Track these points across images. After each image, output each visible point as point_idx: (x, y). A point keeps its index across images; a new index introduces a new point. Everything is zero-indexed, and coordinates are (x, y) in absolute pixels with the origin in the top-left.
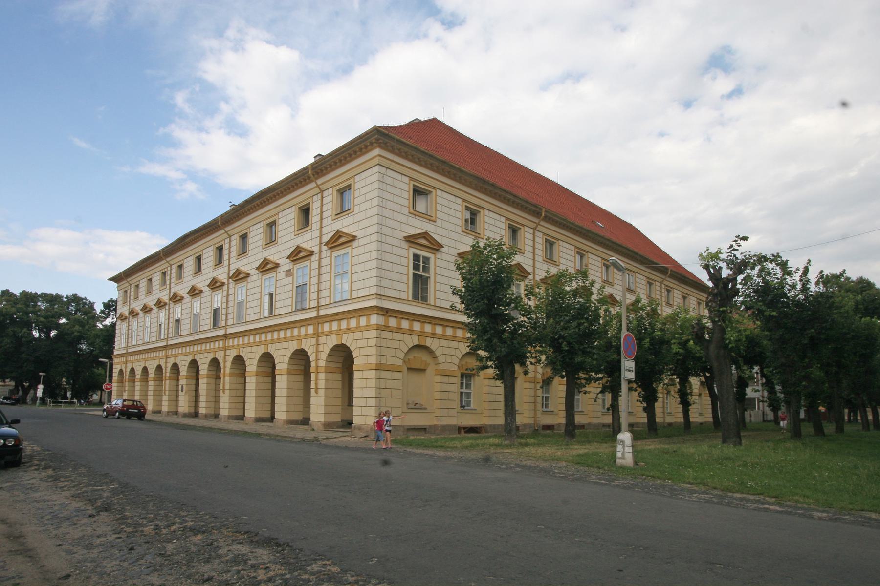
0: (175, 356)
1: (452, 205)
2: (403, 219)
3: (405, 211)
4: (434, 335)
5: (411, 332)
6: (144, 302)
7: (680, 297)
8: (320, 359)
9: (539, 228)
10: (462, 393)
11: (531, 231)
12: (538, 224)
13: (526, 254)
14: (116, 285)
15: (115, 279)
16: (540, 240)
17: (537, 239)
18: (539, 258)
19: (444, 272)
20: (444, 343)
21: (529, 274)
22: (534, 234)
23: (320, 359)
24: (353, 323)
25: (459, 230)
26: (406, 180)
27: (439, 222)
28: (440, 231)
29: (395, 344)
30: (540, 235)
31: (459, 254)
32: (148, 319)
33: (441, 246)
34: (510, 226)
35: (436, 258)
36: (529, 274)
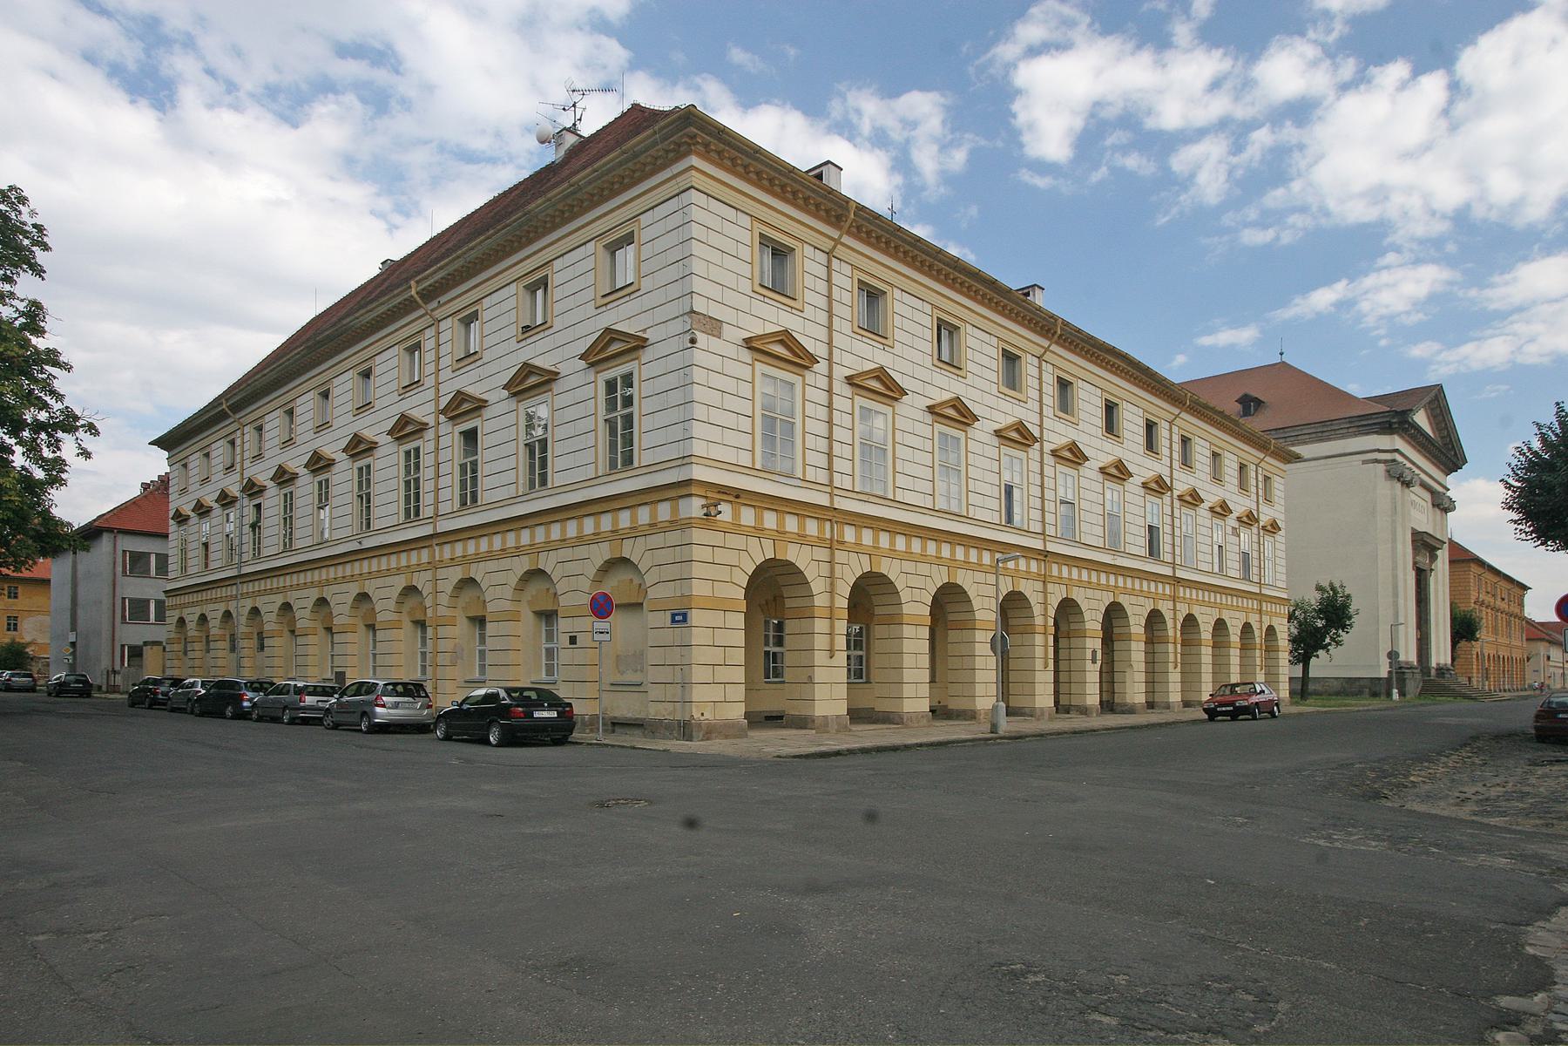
0: (183, 606)
1: (729, 229)
2: (743, 303)
3: (928, 362)
4: (892, 554)
5: (758, 531)
6: (221, 485)
7: (1208, 453)
8: (1042, 614)
9: (1178, 421)
10: (767, 653)
11: (822, 258)
12: (837, 242)
13: (1030, 404)
14: (166, 454)
15: (160, 443)
16: (844, 279)
17: (1045, 377)
18: (1176, 465)
19: (910, 440)
20: (909, 566)
21: (814, 360)
22: (1040, 367)
23: (1042, 614)
24: (644, 515)
25: (746, 286)
26: (745, 221)
27: (898, 348)
28: (975, 395)
29: (731, 557)
30: (847, 269)
31: (747, 341)
32: (206, 527)
33: (904, 392)
34: (764, 240)
35: (804, 384)
36: (814, 360)
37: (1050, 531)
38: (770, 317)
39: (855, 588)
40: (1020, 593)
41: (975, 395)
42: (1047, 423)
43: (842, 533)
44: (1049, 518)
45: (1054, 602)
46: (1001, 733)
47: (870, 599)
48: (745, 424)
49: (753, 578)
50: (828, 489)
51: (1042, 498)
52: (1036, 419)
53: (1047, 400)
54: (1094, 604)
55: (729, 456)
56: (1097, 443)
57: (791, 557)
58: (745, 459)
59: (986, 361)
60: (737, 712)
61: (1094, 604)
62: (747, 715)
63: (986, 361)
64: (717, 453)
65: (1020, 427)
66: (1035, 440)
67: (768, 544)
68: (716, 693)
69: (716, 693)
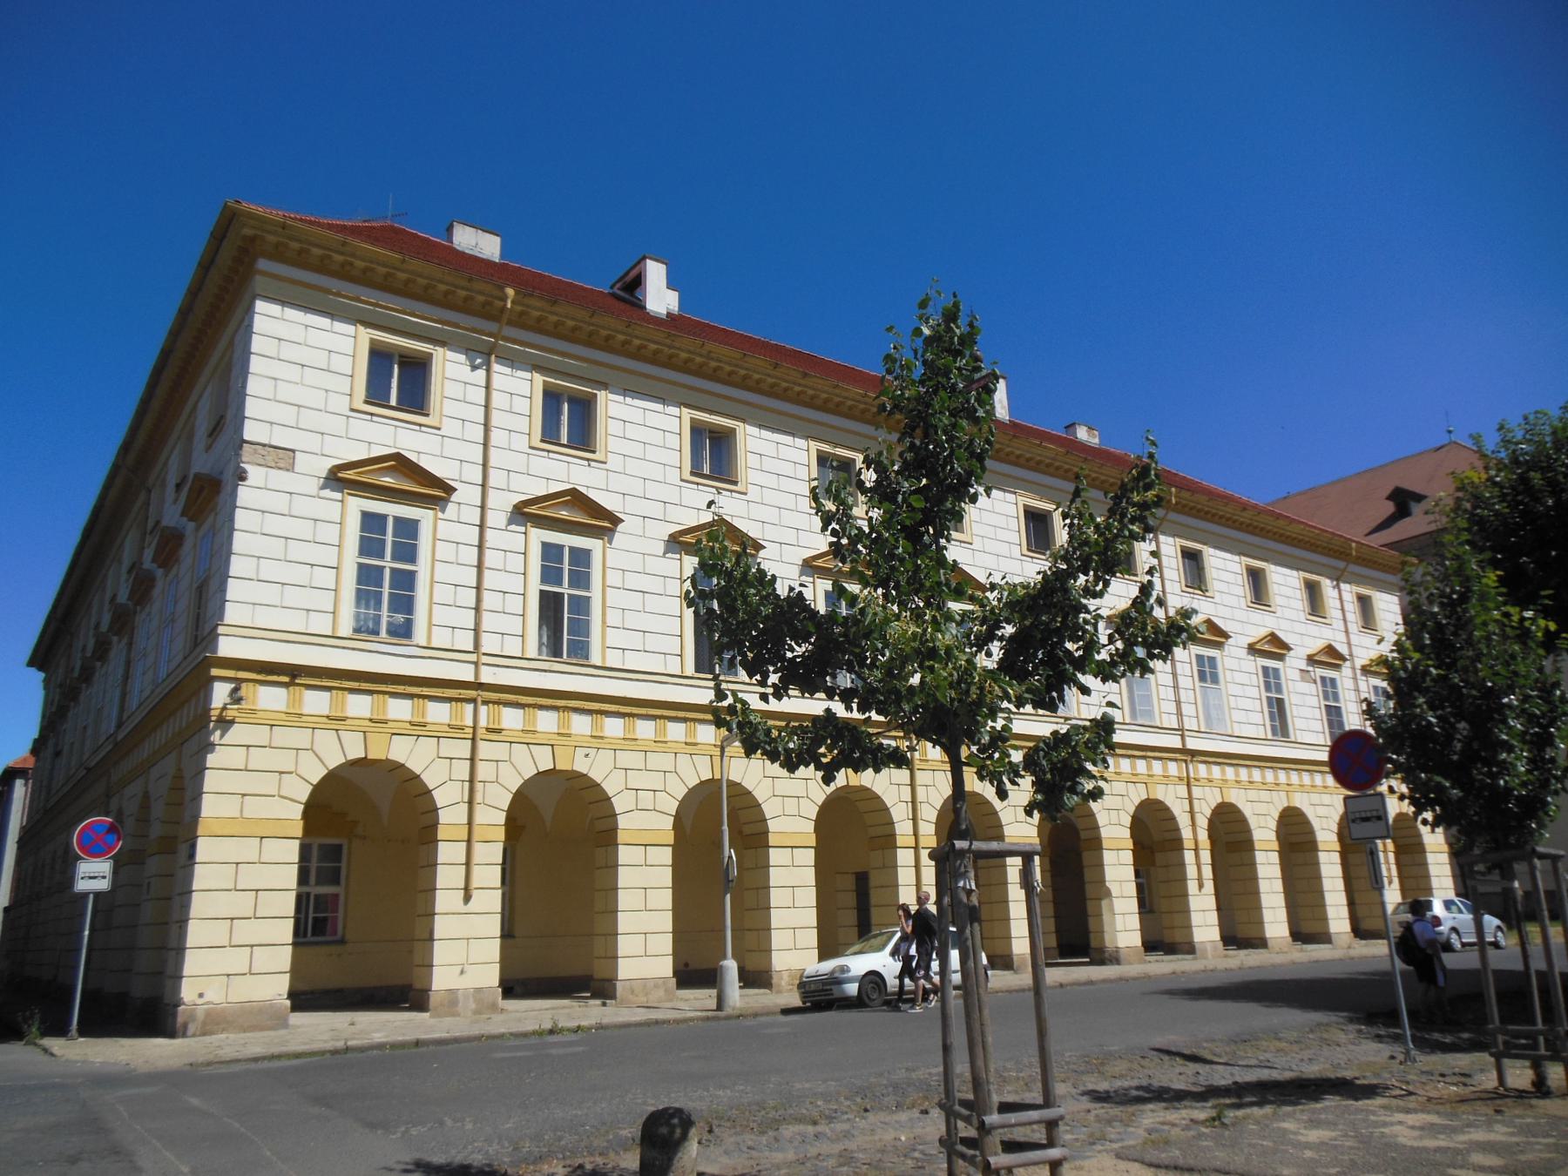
2: (671, 494)
5: (337, 721)
25: (674, 476)
28: (1223, 611)
37: (1190, 724)
38: (388, 434)
39: (1211, 821)
40: (1232, 805)
41: (1284, 625)
42: (1354, 639)
43: (1196, 771)
44: (1188, 709)
45: (1204, 812)
46: (728, 1011)
47: (1229, 831)
48: (327, 579)
49: (320, 790)
50: (473, 657)
51: (1176, 687)
52: (1342, 637)
53: (1351, 617)
54: (1261, 808)
55: (295, 622)
56: (1241, 615)
57: (581, 766)
58: (322, 625)
59: (1289, 592)
60: (277, 988)
61: (1261, 808)
62: (292, 995)
63: (1289, 592)
64: (265, 619)
65: (1330, 650)
66: (1345, 660)
67: (1283, 794)
68: (237, 960)
69: (237, 960)
